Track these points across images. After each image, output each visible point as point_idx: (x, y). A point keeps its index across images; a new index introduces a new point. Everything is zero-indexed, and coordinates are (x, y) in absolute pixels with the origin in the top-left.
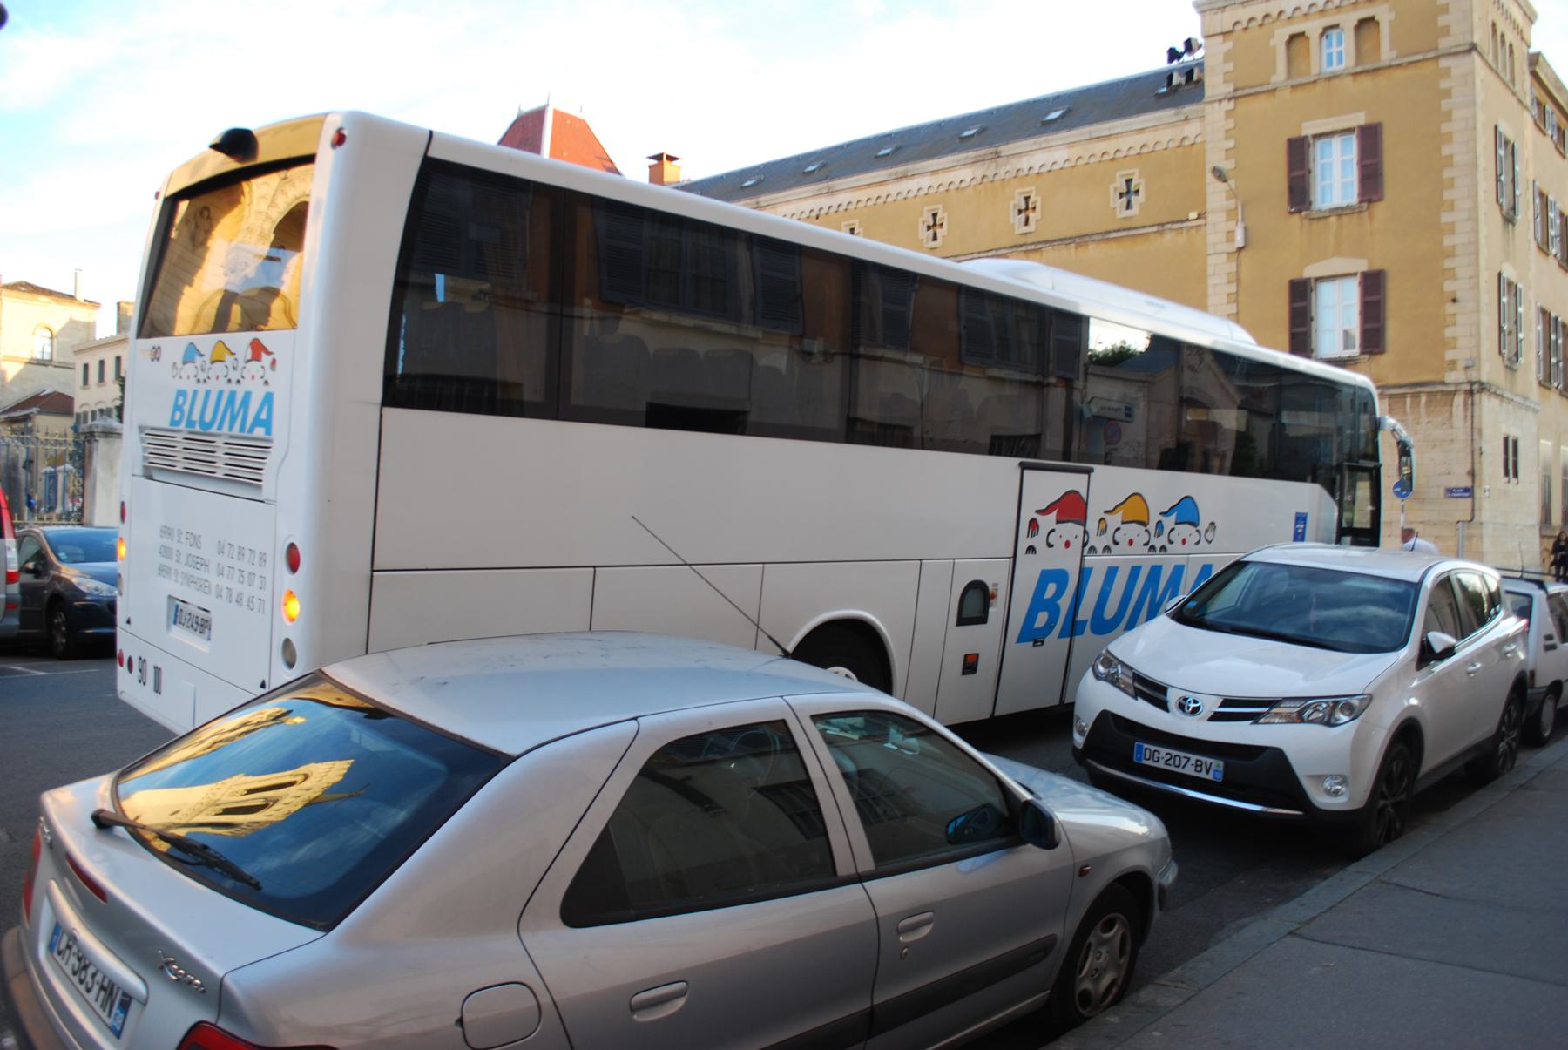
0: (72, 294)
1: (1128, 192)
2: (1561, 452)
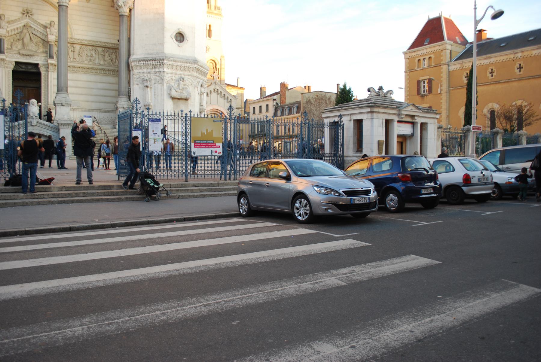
0: (237, 85)
1: (492, 72)
2: (35, 188)
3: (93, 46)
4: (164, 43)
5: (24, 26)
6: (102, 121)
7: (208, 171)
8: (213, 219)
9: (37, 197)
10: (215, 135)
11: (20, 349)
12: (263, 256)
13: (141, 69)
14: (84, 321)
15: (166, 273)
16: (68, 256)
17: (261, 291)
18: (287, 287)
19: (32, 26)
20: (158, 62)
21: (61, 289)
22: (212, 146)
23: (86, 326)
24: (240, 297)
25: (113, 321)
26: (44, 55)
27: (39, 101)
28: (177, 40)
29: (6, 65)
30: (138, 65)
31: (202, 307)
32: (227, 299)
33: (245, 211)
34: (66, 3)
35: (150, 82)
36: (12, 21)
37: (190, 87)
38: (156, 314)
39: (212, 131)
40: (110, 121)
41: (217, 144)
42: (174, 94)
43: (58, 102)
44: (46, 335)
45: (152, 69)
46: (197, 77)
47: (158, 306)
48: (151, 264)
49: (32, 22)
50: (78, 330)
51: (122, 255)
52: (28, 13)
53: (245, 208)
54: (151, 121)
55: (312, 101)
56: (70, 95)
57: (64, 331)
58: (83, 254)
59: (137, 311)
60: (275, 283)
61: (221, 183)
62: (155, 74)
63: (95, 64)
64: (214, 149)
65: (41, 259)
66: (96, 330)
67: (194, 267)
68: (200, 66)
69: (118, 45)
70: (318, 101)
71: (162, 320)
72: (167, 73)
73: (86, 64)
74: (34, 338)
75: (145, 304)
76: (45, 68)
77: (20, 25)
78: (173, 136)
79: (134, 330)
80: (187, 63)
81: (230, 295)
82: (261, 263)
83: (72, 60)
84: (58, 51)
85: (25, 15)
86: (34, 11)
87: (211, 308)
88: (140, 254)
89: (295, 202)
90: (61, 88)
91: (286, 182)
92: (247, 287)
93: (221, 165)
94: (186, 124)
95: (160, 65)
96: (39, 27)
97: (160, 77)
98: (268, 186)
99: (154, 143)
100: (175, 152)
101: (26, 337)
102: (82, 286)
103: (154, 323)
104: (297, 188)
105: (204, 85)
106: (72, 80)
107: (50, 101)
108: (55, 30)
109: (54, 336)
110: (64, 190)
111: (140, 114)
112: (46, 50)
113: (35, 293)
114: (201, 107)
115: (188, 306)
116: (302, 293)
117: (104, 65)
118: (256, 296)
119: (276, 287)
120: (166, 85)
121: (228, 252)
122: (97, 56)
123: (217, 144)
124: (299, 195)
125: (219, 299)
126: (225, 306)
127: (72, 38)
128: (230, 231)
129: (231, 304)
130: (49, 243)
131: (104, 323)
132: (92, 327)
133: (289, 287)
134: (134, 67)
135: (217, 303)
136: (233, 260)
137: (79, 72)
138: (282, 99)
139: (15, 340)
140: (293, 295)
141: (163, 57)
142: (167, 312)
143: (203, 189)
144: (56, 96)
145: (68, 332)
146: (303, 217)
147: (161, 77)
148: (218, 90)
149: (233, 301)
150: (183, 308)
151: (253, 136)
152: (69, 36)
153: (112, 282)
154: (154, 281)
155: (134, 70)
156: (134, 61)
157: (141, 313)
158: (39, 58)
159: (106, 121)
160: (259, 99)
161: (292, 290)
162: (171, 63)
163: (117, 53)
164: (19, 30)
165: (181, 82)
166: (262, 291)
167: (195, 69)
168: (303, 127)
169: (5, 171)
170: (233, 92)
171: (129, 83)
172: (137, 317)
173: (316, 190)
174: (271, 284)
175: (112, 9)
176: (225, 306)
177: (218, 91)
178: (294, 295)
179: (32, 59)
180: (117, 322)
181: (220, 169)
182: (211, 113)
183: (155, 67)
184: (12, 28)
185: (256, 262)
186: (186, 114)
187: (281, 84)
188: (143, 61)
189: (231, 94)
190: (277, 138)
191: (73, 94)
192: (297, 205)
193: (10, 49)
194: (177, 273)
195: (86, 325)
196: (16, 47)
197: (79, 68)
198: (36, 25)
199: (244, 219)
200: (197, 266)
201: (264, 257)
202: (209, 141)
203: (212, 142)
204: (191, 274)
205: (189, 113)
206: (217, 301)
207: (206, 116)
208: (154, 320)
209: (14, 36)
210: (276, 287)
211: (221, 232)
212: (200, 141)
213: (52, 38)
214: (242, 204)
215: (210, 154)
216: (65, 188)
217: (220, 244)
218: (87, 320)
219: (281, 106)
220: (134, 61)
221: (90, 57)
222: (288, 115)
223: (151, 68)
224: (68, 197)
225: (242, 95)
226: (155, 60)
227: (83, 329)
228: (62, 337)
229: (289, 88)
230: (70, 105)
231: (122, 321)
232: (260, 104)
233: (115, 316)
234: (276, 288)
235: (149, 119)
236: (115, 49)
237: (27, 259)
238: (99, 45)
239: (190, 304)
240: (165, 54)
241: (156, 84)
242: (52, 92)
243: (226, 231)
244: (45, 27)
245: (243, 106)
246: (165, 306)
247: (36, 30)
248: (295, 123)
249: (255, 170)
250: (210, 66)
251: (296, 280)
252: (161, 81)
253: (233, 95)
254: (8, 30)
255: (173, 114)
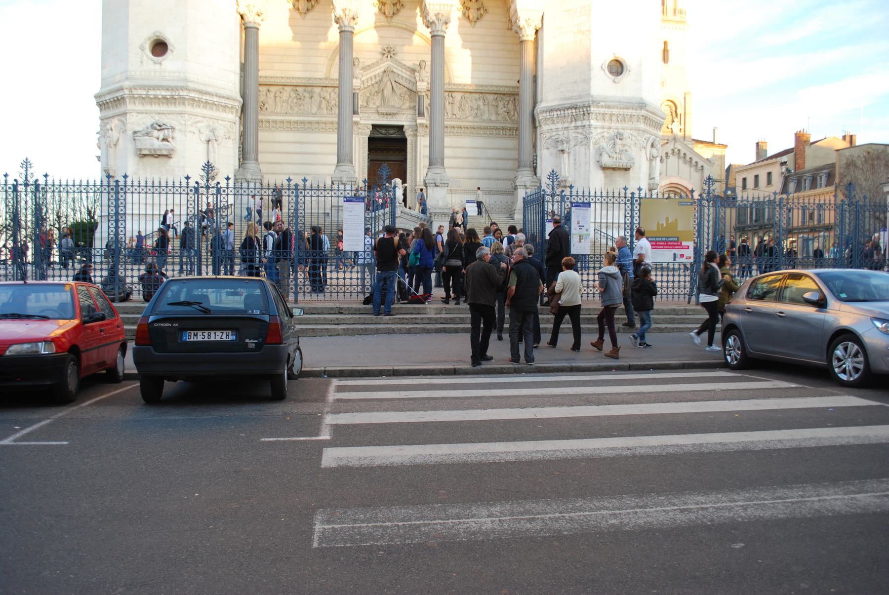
0: (712, 141)
3: (481, 93)
4: (590, 79)
5: (385, 71)
6: (492, 208)
7: (667, 288)
8: (678, 370)
9: (406, 321)
10: (680, 227)
11: (408, 539)
12: (777, 439)
13: (553, 123)
14: (492, 509)
15: (611, 452)
16: (460, 412)
17: (780, 498)
18: (828, 498)
19: (395, 70)
20: (581, 110)
21: (455, 459)
22: (676, 245)
23: (497, 519)
24: (742, 504)
25: (537, 517)
26: (411, 112)
27: (404, 181)
28: (611, 72)
29: (360, 131)
30: (548, 117)
31: (677, 512)
32: (719, 505)
33: (736, 360)
34: (442, 31)
35: (567, 143)
36: (369, 66)
37: (633, 148)
38: (601, 514)
39: (676, 220)
40: (504, 208)
41: (684, 243)
42: (606, 161)
43: (430, 182)
44: (441, 523)
45: (571, 122)
46: (644, 131)
47: (604, 501)
48: (585, 435)
49: (396, 66)
50: (485, 523)
51: (539, 416)
52: (389, 52)
53: (737, 353)
54: (575, 206)
55: (859, 163)
56: (446, 170)
57: (466, 521)
58: (480, 410)
59: (571, 506)
60: (804, 487)
61: (691, 310)
62: (575, 131)
63: (484, 121)
64: (679, 252)
65: (422, 413)
66: (511, 526)
67: (656, 445)
68: (650, 112)
69: (518, 87)
70: (870, 162)
71: (612, 524)
72: (595, 128)
73: (470, 122)
74: (425, 525)
75: (583, 496)
76: (412, 131)
77: (379, 71)
78: (604, 230)
79: (570, 535)
80: (627, 108)
81: (724, 499)
82: (775, 450)
83: (449, 117)
84: (430, 105)
85: (386, 55)
86: (398, 49)
87: (693, 516)
88: (566, 418)
89: (835, 348)
90: (435, 161)
91: (817, 311)
92: (753, 489)
93: (691, 279)
94: (632, 210)
95: (584, 114)
96: (404, 71)
97: (584, 135)
98: (780, 317)
99: (580, 241)
100: (95, 249)
101: (414, 522)
102: (484, 458)
103: (600, 528)
104: (839, 323)
105: (656, 143)
106: (449, 147)
107: (418, 180)
108: (427, 73)
109: (453, 527)
110: (444, 312)
111: (558, 195)
112: (414, 104)
113: (419, 460)
114: (651, 182)
115: (652, 508)
116: (859, 511)
117: (497, 121)
118: (772, 505)
119: (807, 495)
120: (594, 147)
121: (714, 427)
122: (486, 108)
123: (684, 243)
124: (844, 336)
125: (706, 503)
126: (717, 517)
127: (449, 84)
128: (713, 392)
129: (727, 514)
130: (428, 390)
131: (523, 517)
132: (506, 520)
133: (833, 497)
134: (542, 121)
135: (702, 509)
136: (723, 441)
137: (296, 129)
138: (799, 161)
139: (401, 524)
140: (842, 512)
141: (589, 101)
142: (620, 514)
143: (659, 319)
144: (428, 172)
145: (472, 523)
146: (851, 376)
147: (585, 134)
148: (679, 150)
149: (730, 509)
150: (645, 510)
151: (741, 229)
152: (447, 81)
153: (528, 457)
154: (593, 462)
155: (543, 126)
156: (543, 112)
157: (577, 509)
158: (405, 116)
159: (498, 208)
160: (754, 163)
161: (839, 503)
162: (602, 110)
163: (516, 101)
164: (378, 79)
165: (618, 141)
166: (782, 499)
167: (641, 117)
168: (846, 211)
169: (307, 285)
170: (706, 152)
171: (535, 146)
172: (572, 514)
173: (878, 328)
174: (798, 488)
175: (509, 33)
176: (717, 517)
177: (679, 153)
178: (843, 512)
179: (395, 119)
180: (542, 519)
181: (688, 285)
182: (669, 191)
183: (575, 119)
184: (369, 76)
185: (767, 447)
186: (633, 194)
187: (796, 134)
188: (556, 111)
189: (701, 157)
190: (790, 232)
191: (451, 168)
192: (839, 352)
193: (366, 107)
194: (629, 453)
195: (497, 516)
196: (374, 104)
197: (461, 128)
198: (400, 68)
199: (735, 373)
200: (662, 446)
201: (779, 441)
202: (671, 237)
203: (676, 239)
204: (653, 457)
205: (637, 192)
206: (703, 506)
207: (660, 196)
208: (600, 523)
209: (371, 88)
210: (807, 495)
211: (697, 393)
212: (656, 237)
213: (422, 86)
214: (730, 347)
215: (672, 260)
216: (446, 310)
217: (698, 413)
218: (498, 509)
219: (795, 174)
220: (543, 112)
221: (476, 111)
222: (810, 189)
223: (570, 120)
224: (449, 323)
225: (722, 158)
226: (576, 108)
227: (493, 522)
228: (464, 529)
229: (812, 140)
230: (447, 185)
231: (549, 518)
232: (755, 172)
233: (539, 509)
234: (808, 497)
235: (572, 203)
236: (513, 95)
237: (402, 410)
238: (489, 92)
239: (656, 505)
240: (592, 96)
241: (577, 147)
242: (422, 167)
243: (704, 391)
244: (413, 71)
245: (724, 177)
246: (615, 503)
247: (400, 77)
248: (825, 204)
249: (756, 288)
250: (666, 110)
251: (846, 487)
252: (586, 141)
253: (706, 158)
254: (363, 79)
255: (604, 194)
